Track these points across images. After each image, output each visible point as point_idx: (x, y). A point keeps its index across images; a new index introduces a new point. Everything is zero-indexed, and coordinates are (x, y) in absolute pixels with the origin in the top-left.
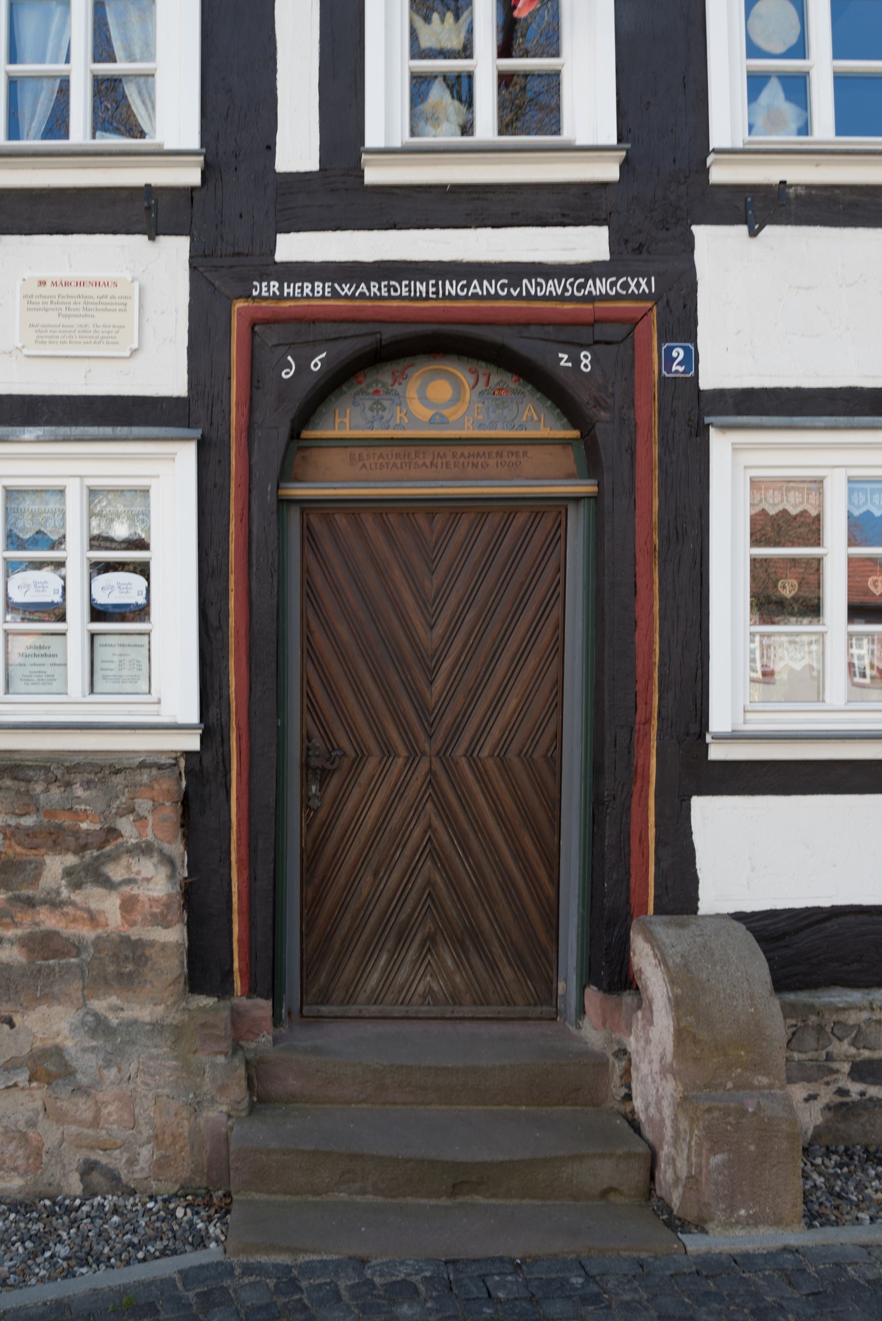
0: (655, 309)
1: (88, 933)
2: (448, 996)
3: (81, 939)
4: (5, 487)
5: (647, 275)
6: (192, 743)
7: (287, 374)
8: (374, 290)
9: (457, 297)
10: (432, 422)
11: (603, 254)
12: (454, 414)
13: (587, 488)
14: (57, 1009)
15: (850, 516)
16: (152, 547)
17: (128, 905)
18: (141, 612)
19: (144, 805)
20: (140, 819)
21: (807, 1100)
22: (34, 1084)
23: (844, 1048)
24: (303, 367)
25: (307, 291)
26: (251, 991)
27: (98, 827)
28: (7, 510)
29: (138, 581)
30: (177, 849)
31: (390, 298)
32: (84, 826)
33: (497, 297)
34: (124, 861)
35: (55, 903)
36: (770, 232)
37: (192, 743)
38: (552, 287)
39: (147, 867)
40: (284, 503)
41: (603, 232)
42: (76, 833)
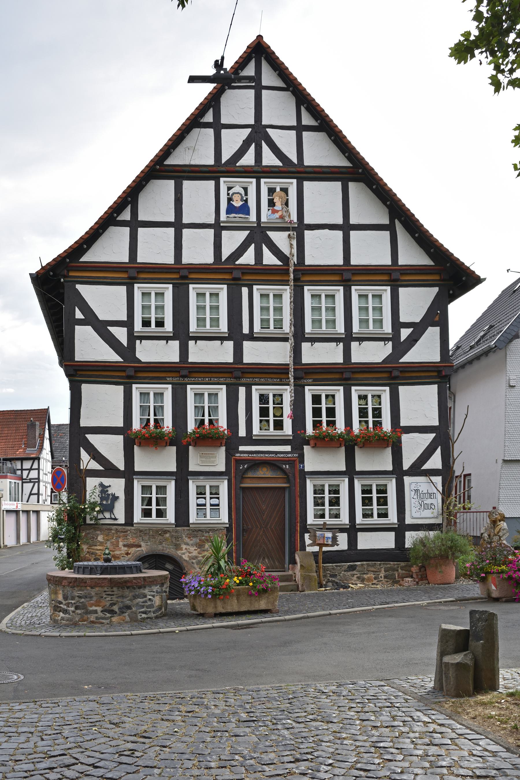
2: (276, 543)
4: (476, 281)
5: (296, 454)
6: (228, 526)
7: (241, 468)
9: (268, 457)
29: (217, 500)
36: (458, 41)
38: (282, 455)
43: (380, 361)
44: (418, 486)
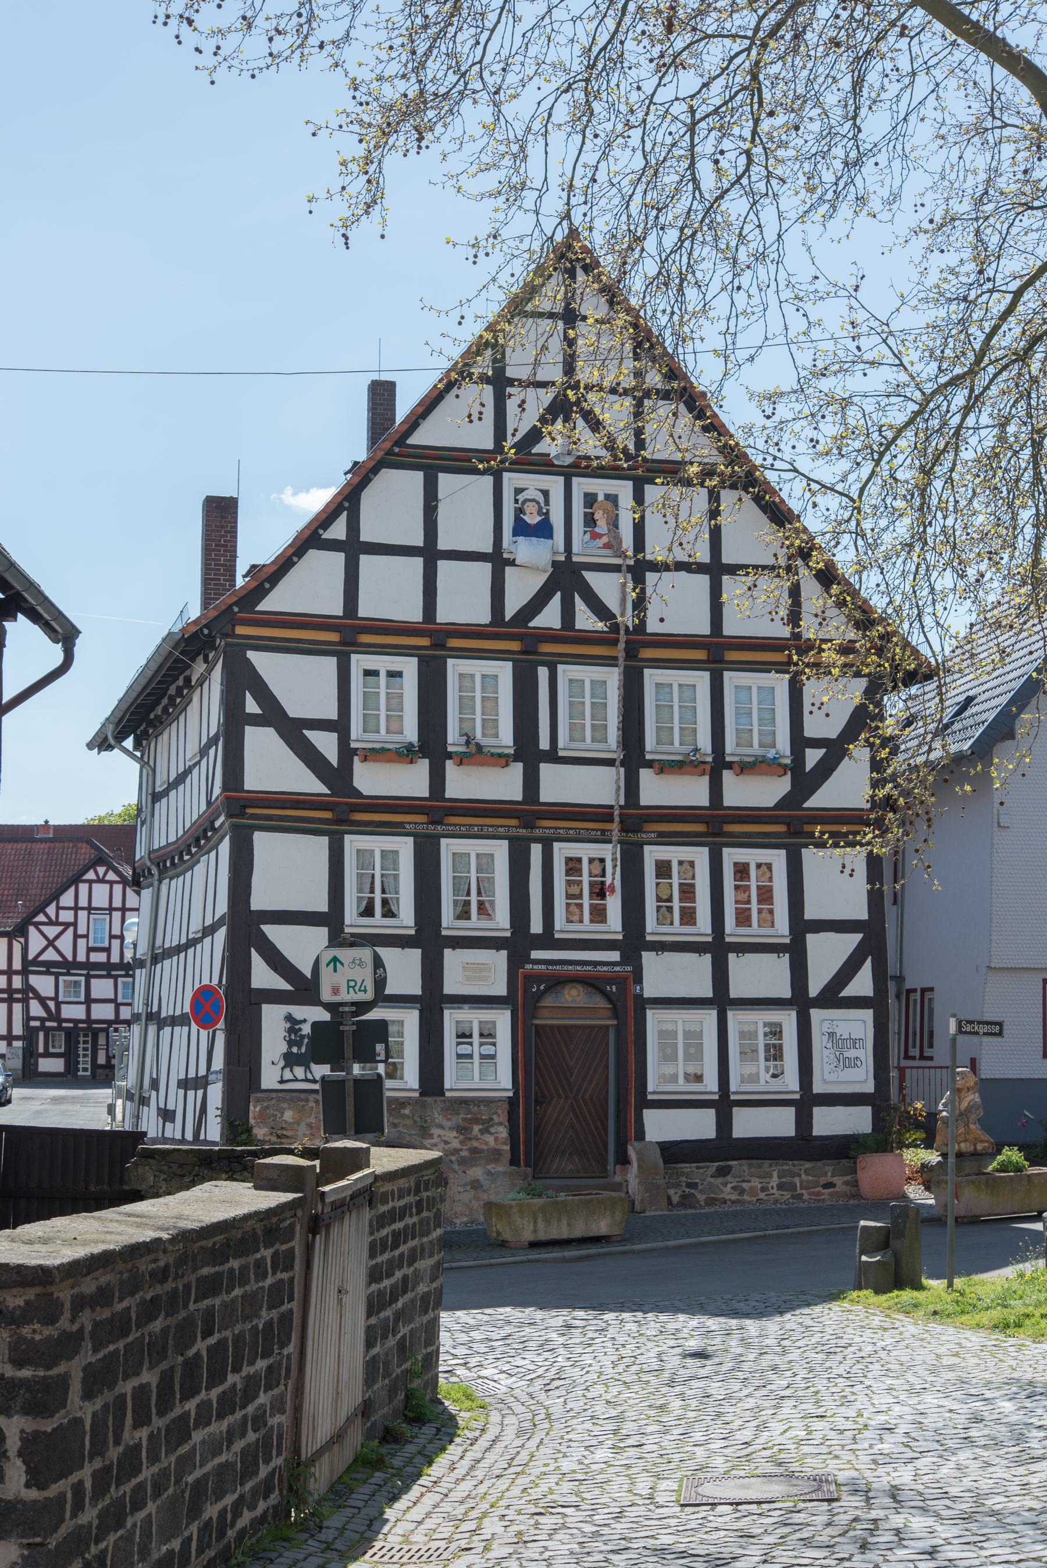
1: (485, 1147)
6: (511, 1094)
12: (578, 999)
13: (615, 1022)
17: (496, 1139)
18: (493, 1057)
23: (684, 1179)
26: (526, 1166)
35: (477, 1139)
38: (605, 968)
39: (501, 1129)
41: (618, 953)
43: (771, 805)
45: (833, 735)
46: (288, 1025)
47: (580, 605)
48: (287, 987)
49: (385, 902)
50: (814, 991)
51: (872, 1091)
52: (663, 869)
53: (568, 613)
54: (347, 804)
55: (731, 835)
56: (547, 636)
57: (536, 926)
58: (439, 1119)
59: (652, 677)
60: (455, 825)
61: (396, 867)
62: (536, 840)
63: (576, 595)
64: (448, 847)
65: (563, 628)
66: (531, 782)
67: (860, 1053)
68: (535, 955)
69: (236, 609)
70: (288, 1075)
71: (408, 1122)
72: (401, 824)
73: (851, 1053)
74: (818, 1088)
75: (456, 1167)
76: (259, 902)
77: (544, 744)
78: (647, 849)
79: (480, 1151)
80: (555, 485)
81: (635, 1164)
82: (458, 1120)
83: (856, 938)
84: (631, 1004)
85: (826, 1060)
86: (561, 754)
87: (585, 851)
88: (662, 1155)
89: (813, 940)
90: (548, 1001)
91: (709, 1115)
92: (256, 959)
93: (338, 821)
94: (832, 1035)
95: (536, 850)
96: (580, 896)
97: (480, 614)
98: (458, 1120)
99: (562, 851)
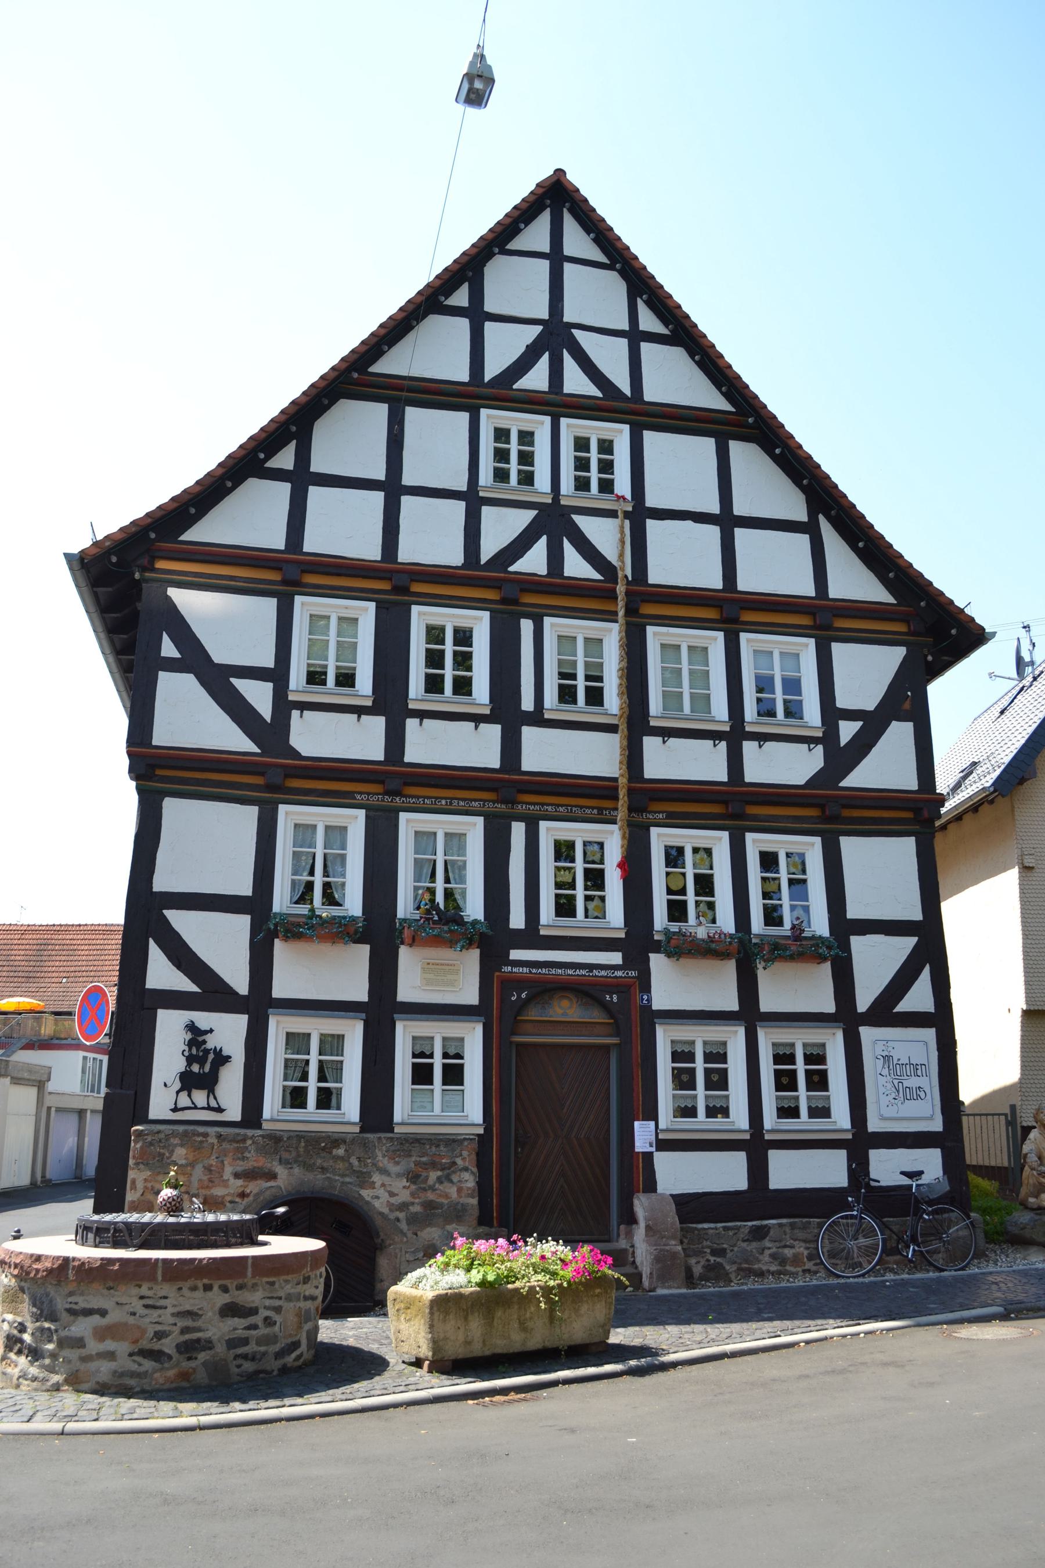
0: (637, 983)
1: (446, 1202)
3: (443, 1203)
6: (481, 1131)
7: (513, 999)
8: (544, 971)
9: (572, 975)
10: (563, 1015)
11: (621, 962)
14: (434, 1229)
15: (704, 1052)
16: (465, 1058)
17: (460, 1190)
19: (465, 1153)
20: (464, 1159)
21: (696, 1263)
22: (425, 1258)
24: (519, 996)
25: (521, 970)
27: (449, 1161)
28: (413, 1044)
30: (475, 1170)
31: (549, 974)
32: (443, 1161)
33: (585, 975)
34: (458, 1173)
35: (432, 1188)
37: (481, 1131)
38: (603, 973)
39: (466, 1176)
40: (511, 1043)
41: (620, 954)
42: (441, 1164)
43: (802, 782)
44: (890, 1049)
45: (871, 706)
46: (189, 1036)
47: (568, 549)
48: (193, 988)
49: (327, 886)
50: (863, 1005)
51: (941, 1129)
52: (674, 857)
53: (555, 558)
54: (282, 766)
55: (755, 818)
56: (529, 583)
57: (517, 920)
58: (383, 1162)
59: (655, 636)
60: (418, 797)
61: (462, 849)
62: (519, 819)
63: (565, 541)
64: (408, 824)
65: (549, 575)
66: (511, 747)
67: (922, 1082)
68: (515, 955)
69: (153, 536)
70: (184, 1100)
71: (340, 1165)
72: (350, 795)
73: (913, 1082)
74: (874, 1125)
75: (403, 1226)
76: (161, 883)
77: (527, 704)
78: (654, 831)
79: (440, 1206)
80: (541, 425)
81: (642, 1224)
82: (408, 1164)
83: (911, 941)
84: (636, 1016)
85: (882, 1090)
86: (547, 716)
87: (578, 832)
88: (679, 1212)
89: (858, 943)
90: (533, 1014)
91: (738, 1160)
92: (154, 952)
93: (270, 788)
94: (887, 1058)
95: (518, 831)
96: (572, 885)
97: (453, 555)
98: (408, 1164)
99: (549, 832)
